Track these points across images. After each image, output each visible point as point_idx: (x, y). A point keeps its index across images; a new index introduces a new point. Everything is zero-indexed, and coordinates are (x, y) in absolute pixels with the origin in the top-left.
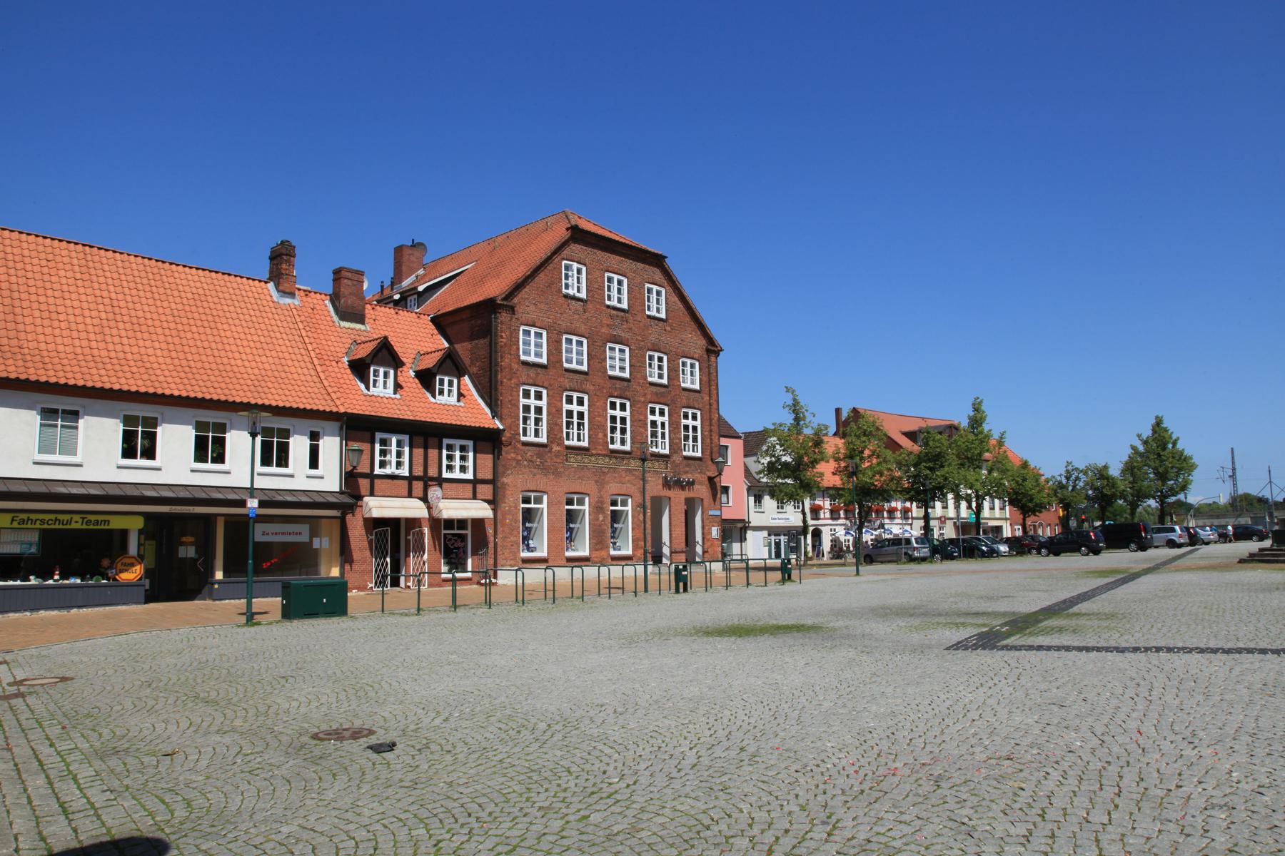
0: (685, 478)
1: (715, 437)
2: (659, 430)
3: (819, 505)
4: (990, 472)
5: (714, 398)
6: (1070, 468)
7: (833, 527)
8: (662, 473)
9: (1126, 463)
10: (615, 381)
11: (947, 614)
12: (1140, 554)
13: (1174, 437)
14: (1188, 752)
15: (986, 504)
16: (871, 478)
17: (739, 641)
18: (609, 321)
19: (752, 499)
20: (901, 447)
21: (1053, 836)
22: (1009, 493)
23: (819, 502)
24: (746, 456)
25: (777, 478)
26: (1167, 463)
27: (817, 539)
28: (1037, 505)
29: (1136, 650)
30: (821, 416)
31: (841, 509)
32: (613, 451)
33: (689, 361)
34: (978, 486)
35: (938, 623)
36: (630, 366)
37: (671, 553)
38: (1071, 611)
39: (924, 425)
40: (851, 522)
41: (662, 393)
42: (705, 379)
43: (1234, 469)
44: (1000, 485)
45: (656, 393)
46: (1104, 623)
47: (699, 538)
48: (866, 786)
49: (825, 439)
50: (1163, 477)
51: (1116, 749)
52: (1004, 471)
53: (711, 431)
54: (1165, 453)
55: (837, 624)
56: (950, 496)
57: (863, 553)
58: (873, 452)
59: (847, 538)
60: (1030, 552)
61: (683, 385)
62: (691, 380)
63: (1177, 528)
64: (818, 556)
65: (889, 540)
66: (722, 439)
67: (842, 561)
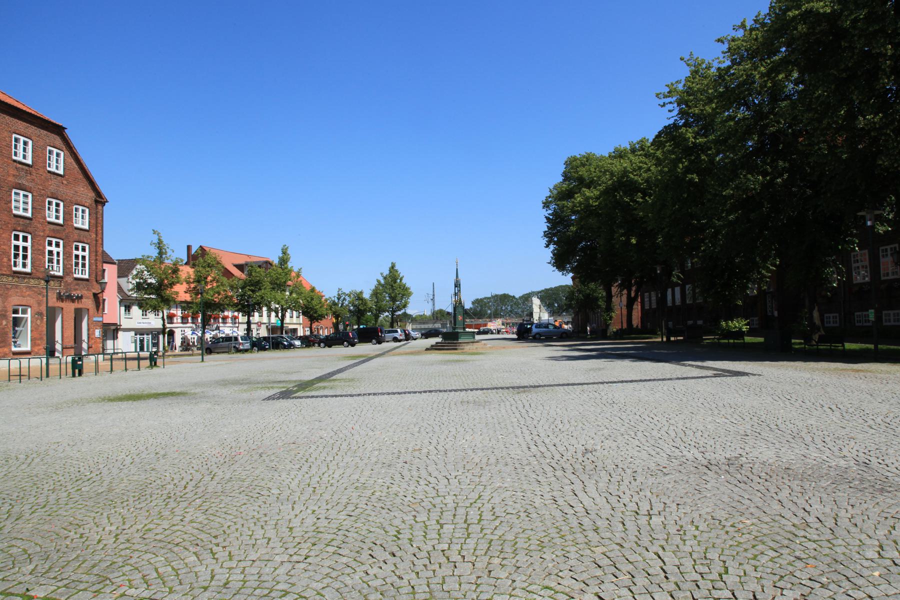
0: (75, 293)
1: (99, 264)
2: (55, 257)
3: (173, 314)
4: (291, 294)
5: (100, 236)
6: (340, 292)
7: (183, 329)
8: (56, 289)
9: (374, 290)
10: (19, 219)
11: (262, 383)
12: (378, 346)
13: (401, 276)
14: (371, 433)
15: (288, 314)
16: (212, 296)
17: (135, 403)
18: (15, 172)
19: (123, 309)
20: (234, 275)
21: (310, 467)
22: (302, 308)
23: (173, 311)
24: (119, 277)
25: (144, 294)
26: (396, 291)
27: (171, 337)
28: (319, 316)
29: (359, 395)
30: (177, 253)
31: (189, 316)
32: (15, 272)
33: (81, 208)
34: (283, 302)
35: (258, 388)
36: (33, 208)
37: (63, 348)
38: (332, 378)
39: (249, 260)
40: (196, 325)
41: (58, 231)
42: (93, 221)
43: (434, 295)
44: (296, 302)
45: (54, 230)
46: (347, 384)
47: (85, 336)
48: (227, 460)
49: (181, 268)
50: (393, 299)
51: (341, 435)
52: (300, 294)
53: (96, 260)
54: (396, 285)
55: (196, 391)
56: (265, 309)
57: (205, 346)
58: (214, 279)
59: (193, 336)
60: (314, 345)
61: (75, 225)
62: (82, 221)
63: (399, 330)
64: (172, 349)
65: (222, 338)
66: (104, 265)
67: (190, 352)
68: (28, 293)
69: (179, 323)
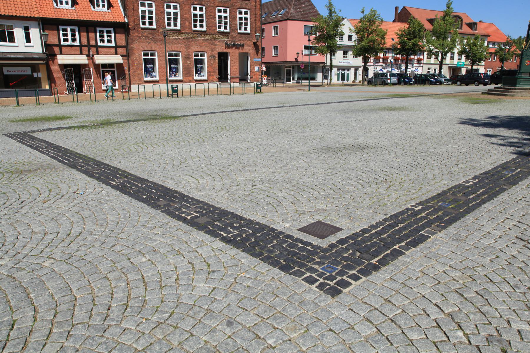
27: (367, 72)
32: (194, 31)
40: (386, 64)
68: (204, 43)
69: (372, 63)
